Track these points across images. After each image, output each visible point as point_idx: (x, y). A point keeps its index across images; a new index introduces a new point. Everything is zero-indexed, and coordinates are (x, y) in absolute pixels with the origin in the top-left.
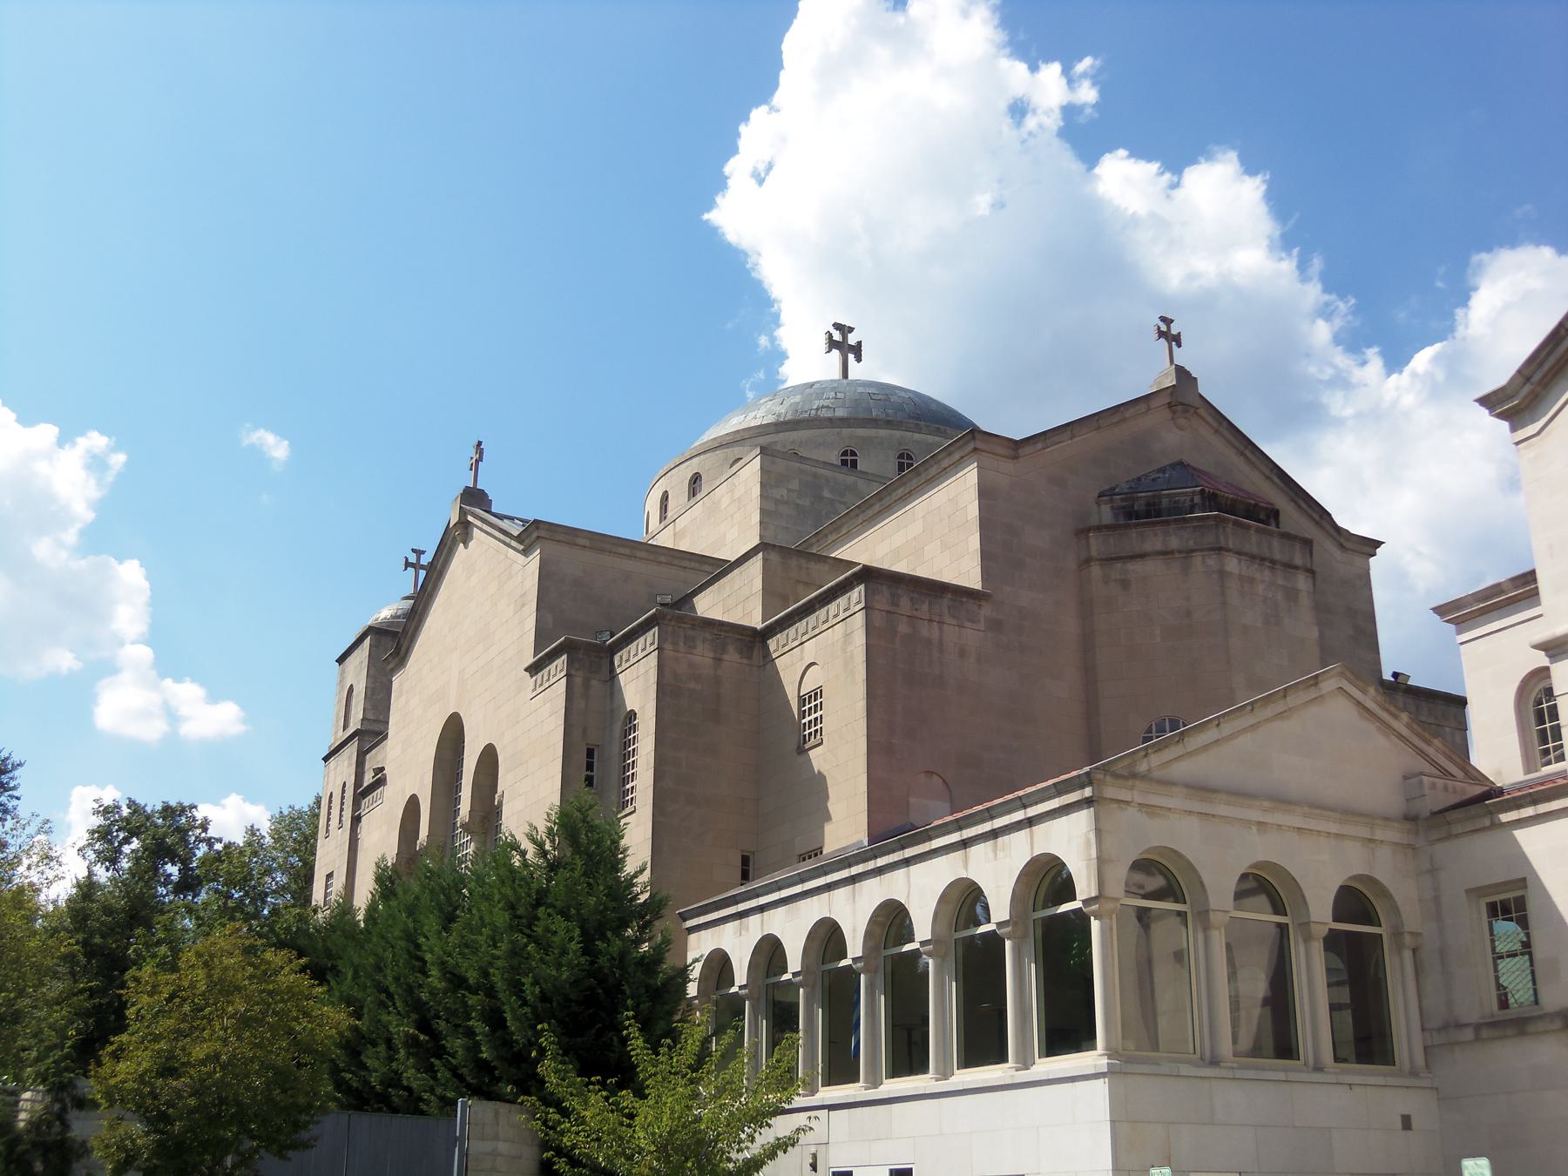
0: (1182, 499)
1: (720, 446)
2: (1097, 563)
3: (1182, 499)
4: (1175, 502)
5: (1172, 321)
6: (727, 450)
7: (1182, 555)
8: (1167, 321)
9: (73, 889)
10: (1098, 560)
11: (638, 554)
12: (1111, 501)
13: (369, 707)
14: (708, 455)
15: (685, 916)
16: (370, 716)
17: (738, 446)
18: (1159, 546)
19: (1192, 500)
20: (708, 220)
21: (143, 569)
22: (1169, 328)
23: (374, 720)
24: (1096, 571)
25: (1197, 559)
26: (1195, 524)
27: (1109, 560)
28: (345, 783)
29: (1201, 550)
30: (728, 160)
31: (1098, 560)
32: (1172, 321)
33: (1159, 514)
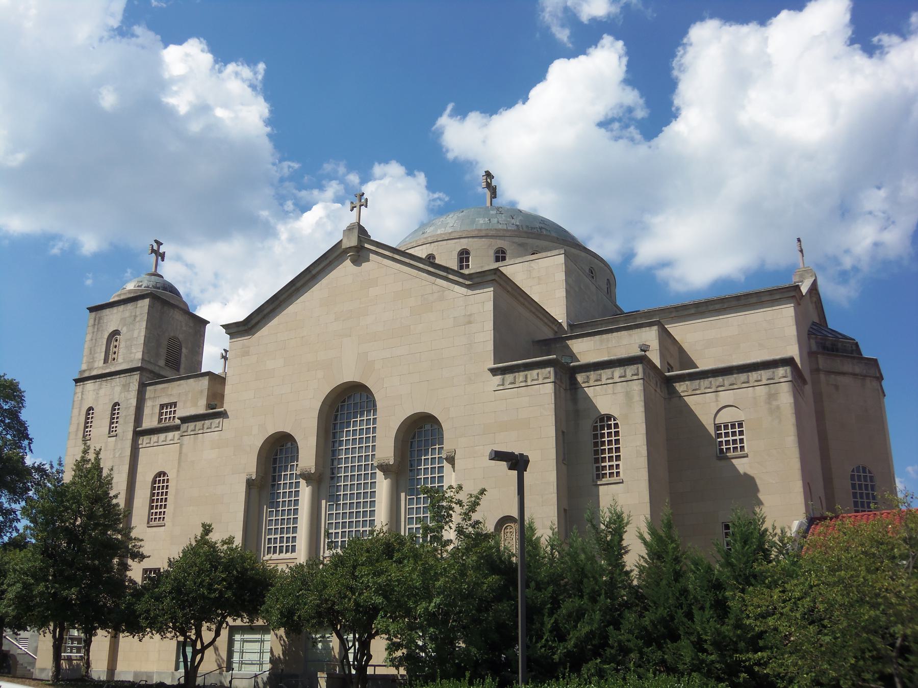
0: (848, 345)
1: (486, 236)
2: (823, 373)
3: (848, 345)
4: (845, 346)
5: (162, 244)
6: (492, 240)
7: (861, 377)
8: (159, 244)
9: (284, 567)
10: (824, 371)
11: (764, 299)
12: (816, 338)
13: (146, 351)
14: (476, 240)
15: (269, 549)
16: (146, 358)
17: (499, 239)
18: (850, 370)
19: (852, 347)
20: (457, 117)
21: (426, 178)
22: (159, 248)
23: (148, 362)
24: (822, 377)
25: (868, 380)
26: (866, 362)
27: (829, 372)
28: (808, 483)
29: (870, 377)
30: (535, 85)
31: (824, 371)
32: (162, 244)
33: (837, 350)
